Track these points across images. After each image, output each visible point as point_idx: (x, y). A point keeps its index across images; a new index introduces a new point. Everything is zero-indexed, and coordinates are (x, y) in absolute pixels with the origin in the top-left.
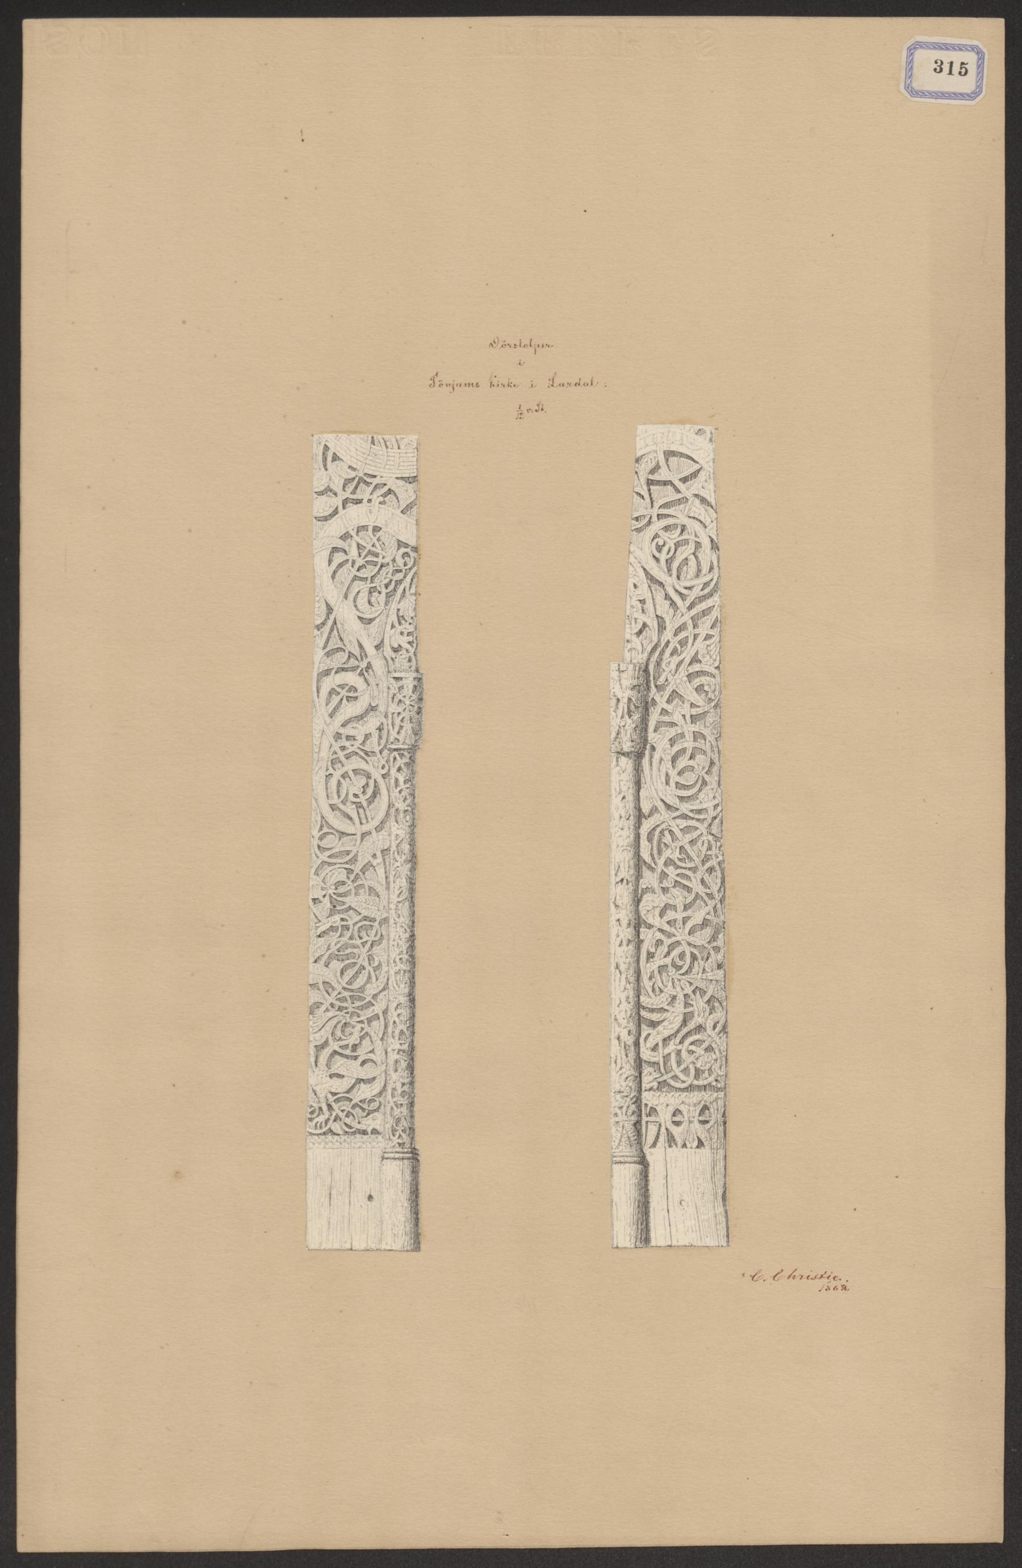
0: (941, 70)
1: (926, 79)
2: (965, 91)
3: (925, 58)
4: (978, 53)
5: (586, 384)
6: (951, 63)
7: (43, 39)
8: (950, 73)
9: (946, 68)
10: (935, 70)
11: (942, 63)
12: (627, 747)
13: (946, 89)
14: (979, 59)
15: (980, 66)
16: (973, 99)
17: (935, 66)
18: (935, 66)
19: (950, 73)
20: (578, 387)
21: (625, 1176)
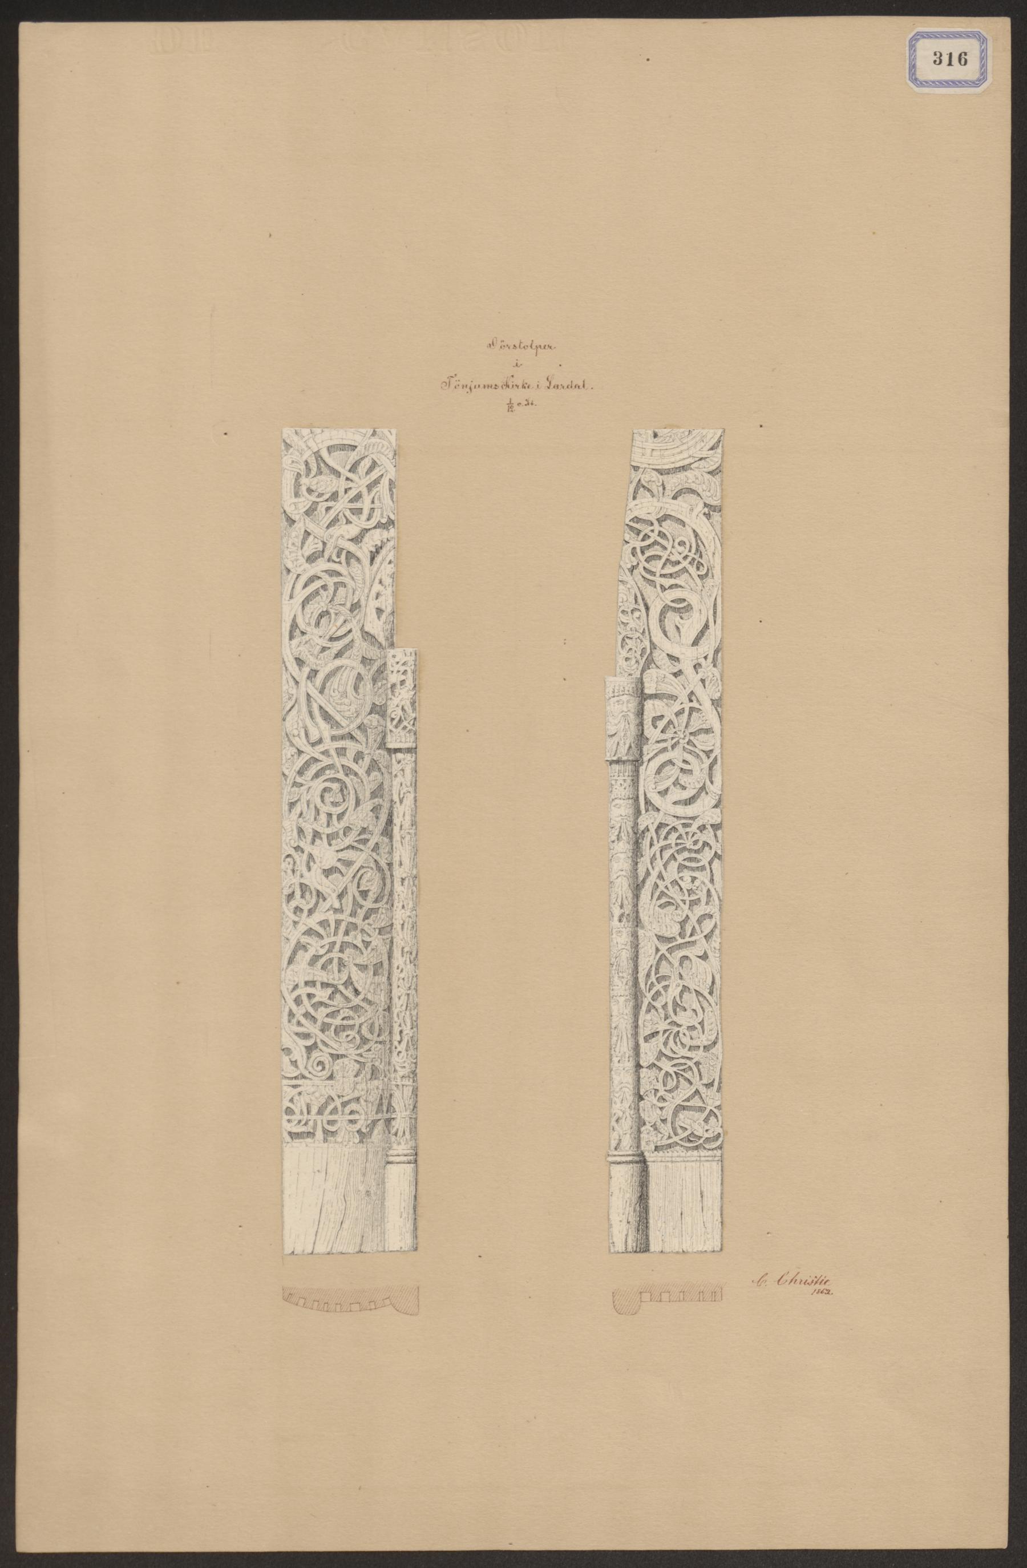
0: (941, 62)
1: (927, 70)
2: (926, 40)
3: (926, 49)
4: (916, 79)
5: (577, 387)
6: (951, 54)
7: (40, 43)
8: (950, 64)
9: (945, 59)
10: (935, 61)
11: (941, 55)
12: (622, 753)
13: (945, 41)
14: (914, 74)
15: (983, 58)
16: (918, 34)
17: (935, 58)
18: (935, 58)
19: (950, 64)
20: (570, 390)
21: (623, 1177)
